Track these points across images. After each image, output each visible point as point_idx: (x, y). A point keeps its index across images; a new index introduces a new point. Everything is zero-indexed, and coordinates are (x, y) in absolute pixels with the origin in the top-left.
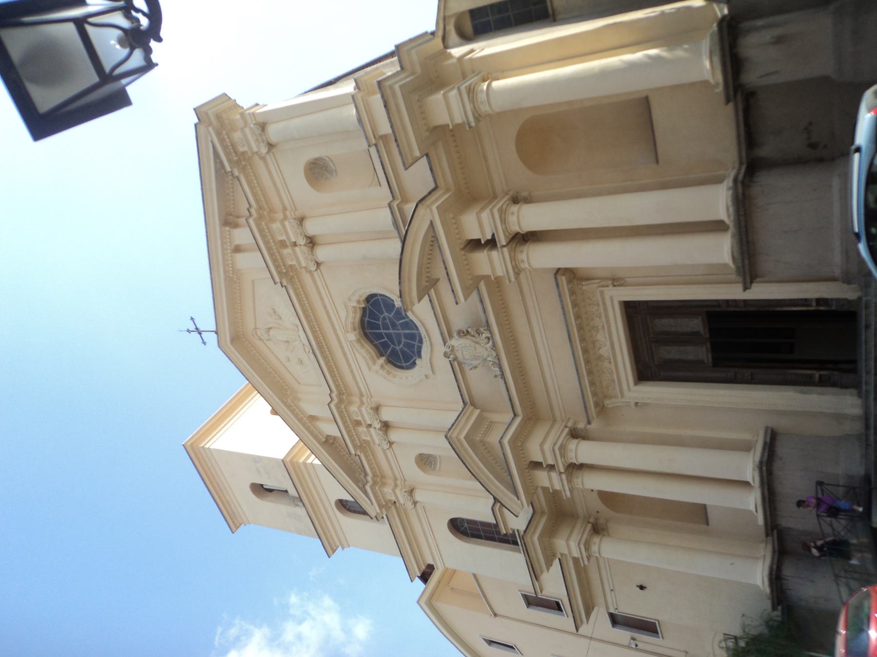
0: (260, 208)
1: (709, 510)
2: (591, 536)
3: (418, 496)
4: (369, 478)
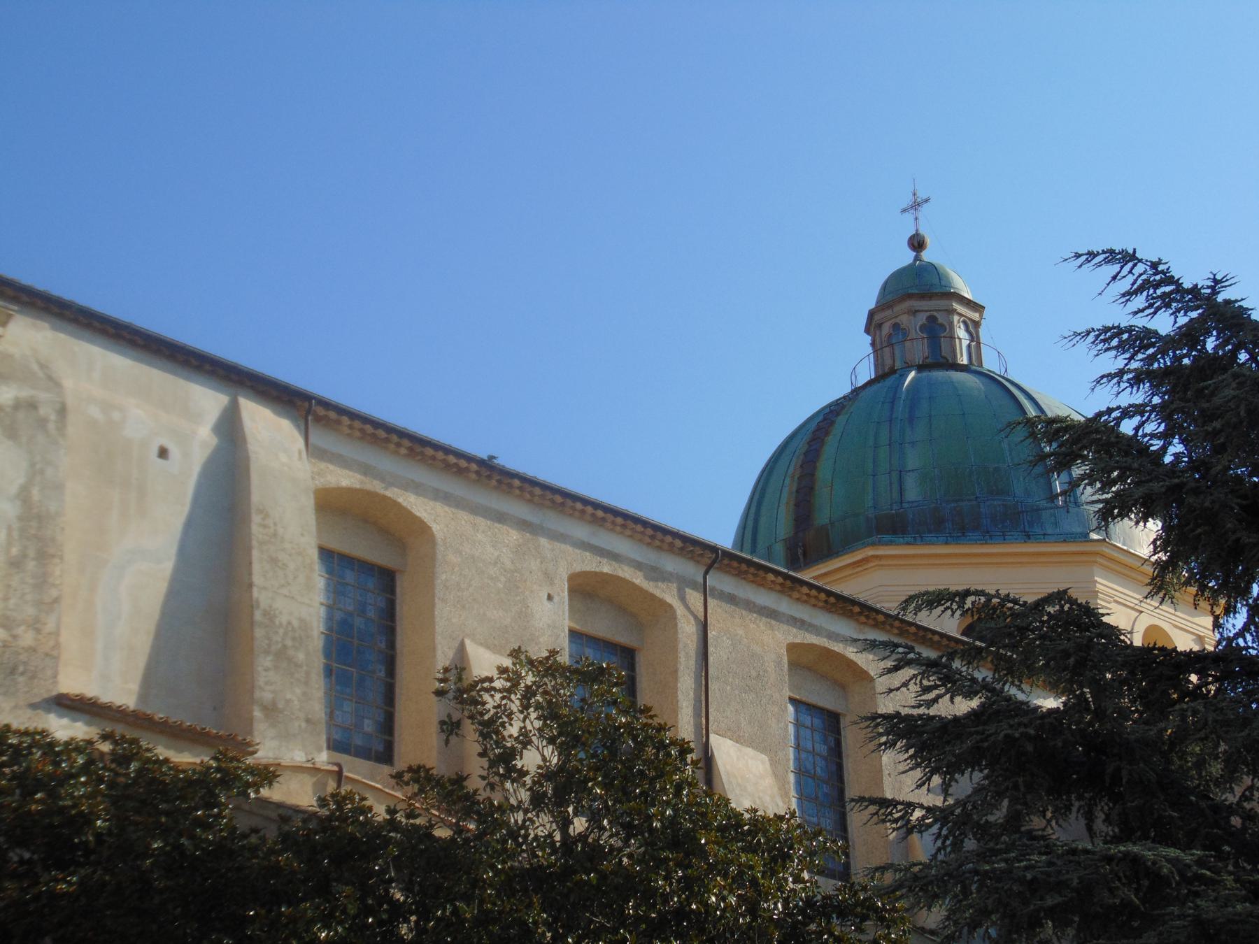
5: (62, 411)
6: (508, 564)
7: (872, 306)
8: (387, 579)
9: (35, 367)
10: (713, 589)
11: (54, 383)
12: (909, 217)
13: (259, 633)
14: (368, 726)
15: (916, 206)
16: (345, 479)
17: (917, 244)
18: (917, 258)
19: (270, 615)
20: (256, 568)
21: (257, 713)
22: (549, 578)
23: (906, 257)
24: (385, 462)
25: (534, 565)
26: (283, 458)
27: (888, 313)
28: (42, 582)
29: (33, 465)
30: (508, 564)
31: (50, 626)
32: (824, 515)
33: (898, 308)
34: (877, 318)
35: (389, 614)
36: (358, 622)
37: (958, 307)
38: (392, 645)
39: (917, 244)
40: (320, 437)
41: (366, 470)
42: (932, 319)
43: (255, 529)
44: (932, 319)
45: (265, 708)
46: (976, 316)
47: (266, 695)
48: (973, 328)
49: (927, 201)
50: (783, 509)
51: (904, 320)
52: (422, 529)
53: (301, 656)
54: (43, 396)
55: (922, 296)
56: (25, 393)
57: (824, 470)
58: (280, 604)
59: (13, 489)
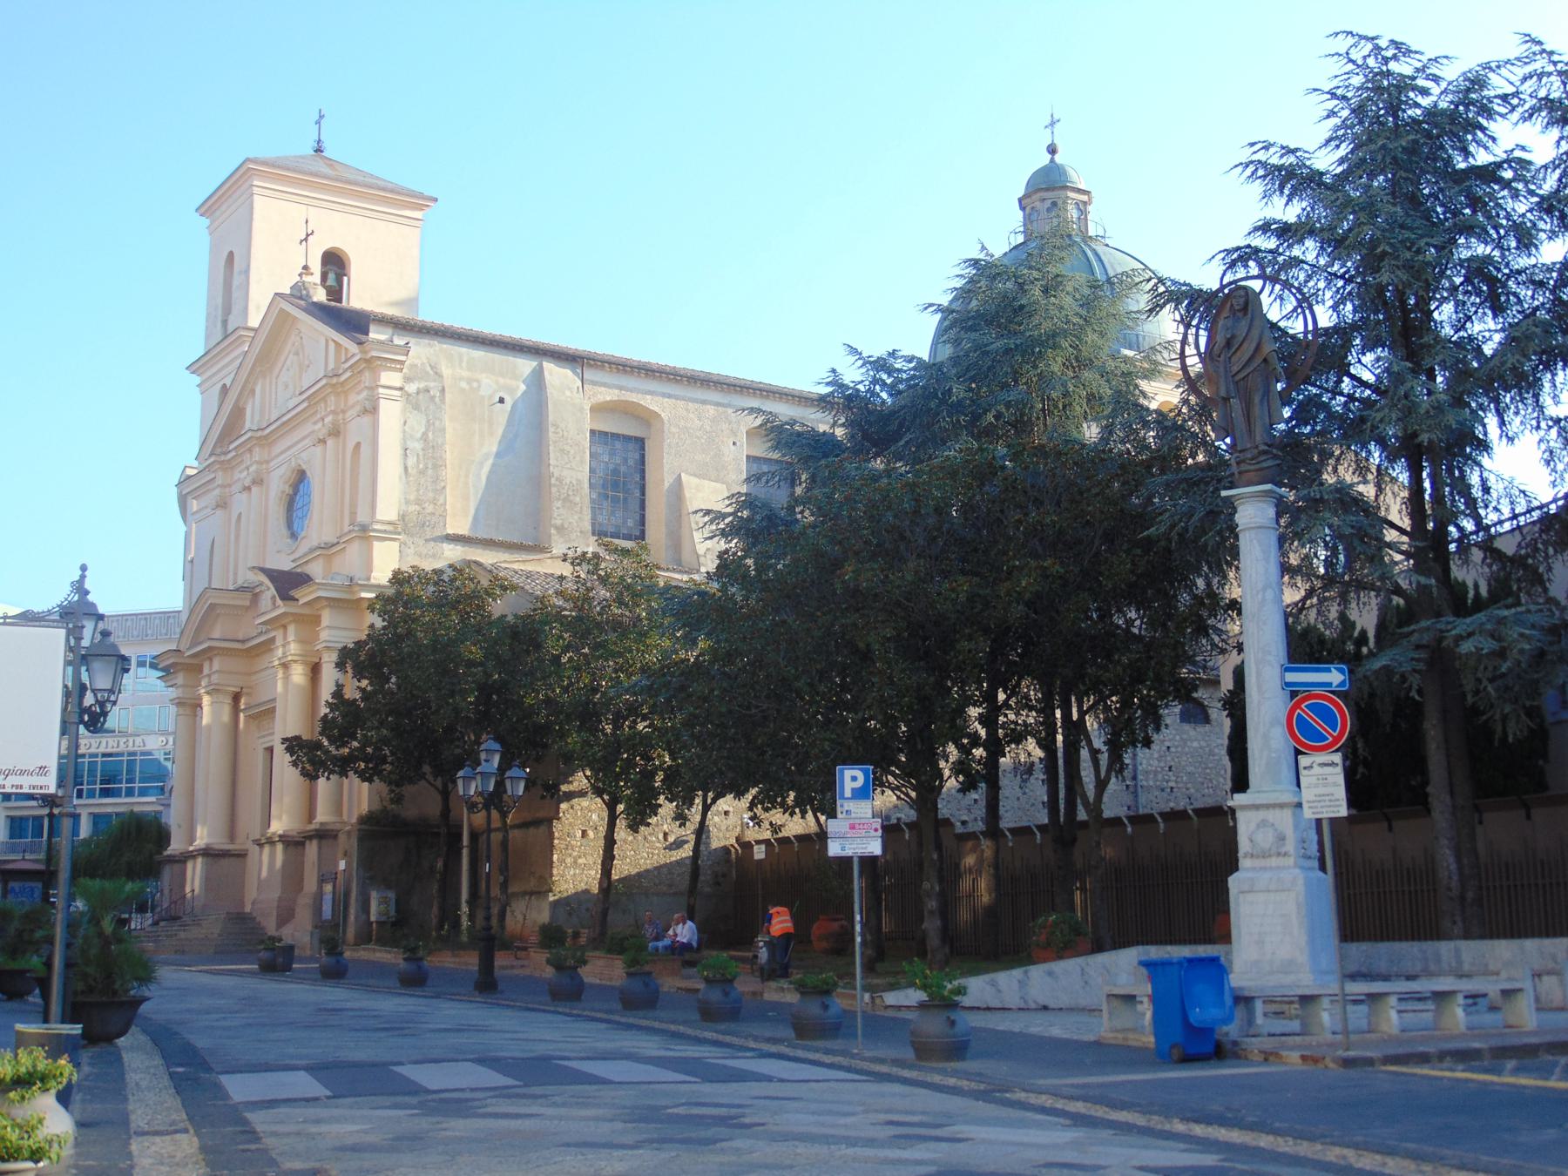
0: (342, 384)
1: (41, 1019)
2: (304, 663)
3: (219, 512)
4: (223, 458)
5: (443, 390)
6: (708, 428)
7: (1021, 193)
8: (640, 442)
9: (429, 369)
11: (438, 375)
12: (1049, 131)
13: (554, 490)
14: (630, 523)
15: (1052, 124)
16: (608, 395)
17: (1052, 150)
18: (1052, 160)
19: (559, 480)
20: (552, 455)
21: (553, 531)
22: (734, 433)
23: (1045, 159)
24: (625, 381)
25: (725, 426)
26: (568, 393)
27: (1028, 200)
28: (436, 480)
29: (428, 421)
30: (708, 428)
31: (441, 501)
33: (1035, 197)
35: (642, 460)
36: (623, 469)
37: (1071, 194)
38: (643, 478)
39: (1052, 150)
40: (588, 374)
41: (621, 388)
42: (1054, 204)
43: (550, 434)
45: (557, 528)
46: (1085, 198)
47: (558, 522)
48: (1083, 208)
51: (1038, 204)
52: (658, 416)
53: (578, 499)
54: (432, 384)
55: (1047, 190)
56: (422, 385)
58: (565, 473)
59: (419, 435)
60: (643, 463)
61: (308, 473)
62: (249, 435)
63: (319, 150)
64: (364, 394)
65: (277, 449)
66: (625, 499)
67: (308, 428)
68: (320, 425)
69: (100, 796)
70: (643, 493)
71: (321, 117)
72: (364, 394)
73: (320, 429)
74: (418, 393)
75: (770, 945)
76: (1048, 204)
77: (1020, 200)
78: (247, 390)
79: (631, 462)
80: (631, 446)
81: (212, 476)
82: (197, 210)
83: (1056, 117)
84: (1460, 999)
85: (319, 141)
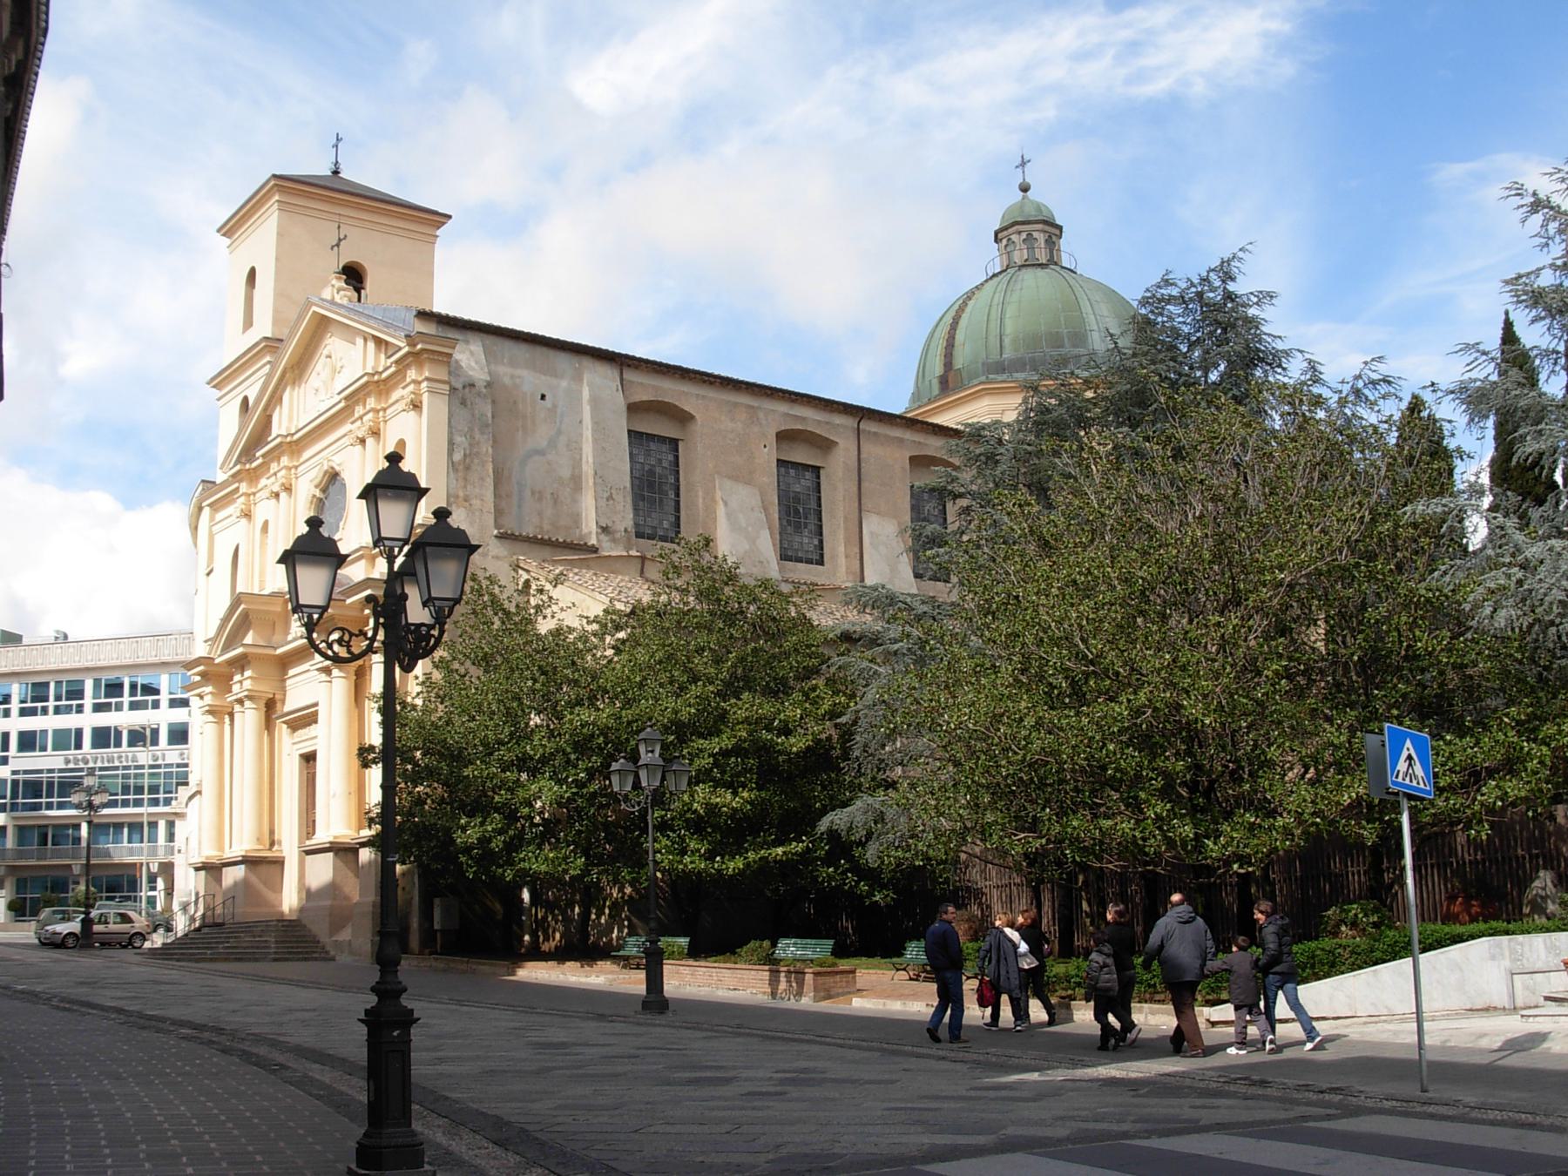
10: (864, 431)
12: (1020, 170)
14: (666, 524)
15: (1023, 164)
32: (959, 363)
34: (1000, 236)
36: (658, 470)
39: (1025, 189)
44: (1029, 235)
49: (1029, 161)
50: (938, 358)
51: (1014, 237)
55: (1023, 223)
57: (960, 336)
60: (677, 465)
61: (343, 475)
62: (279, 440)
63: (336, 172)
64: (411, 387)
65: (307, 455)
66: (661, 500)
67: (347, 427)
68: (273, 479)
69: (149, 805)
70: (678, 495)
71: (208, 574)
72: (411, 387)
73: (359, 429)
74: (464, 387)
75: (604, 913)
76: (1024, 236)
77: (996, 234)
78: (275, 399)
79: (665, 464)
80: (665, 448)
81: (236, 485)
82: (218, 231)
83: (1026, 158)
84: (126, 825)
85: (337, 162)
